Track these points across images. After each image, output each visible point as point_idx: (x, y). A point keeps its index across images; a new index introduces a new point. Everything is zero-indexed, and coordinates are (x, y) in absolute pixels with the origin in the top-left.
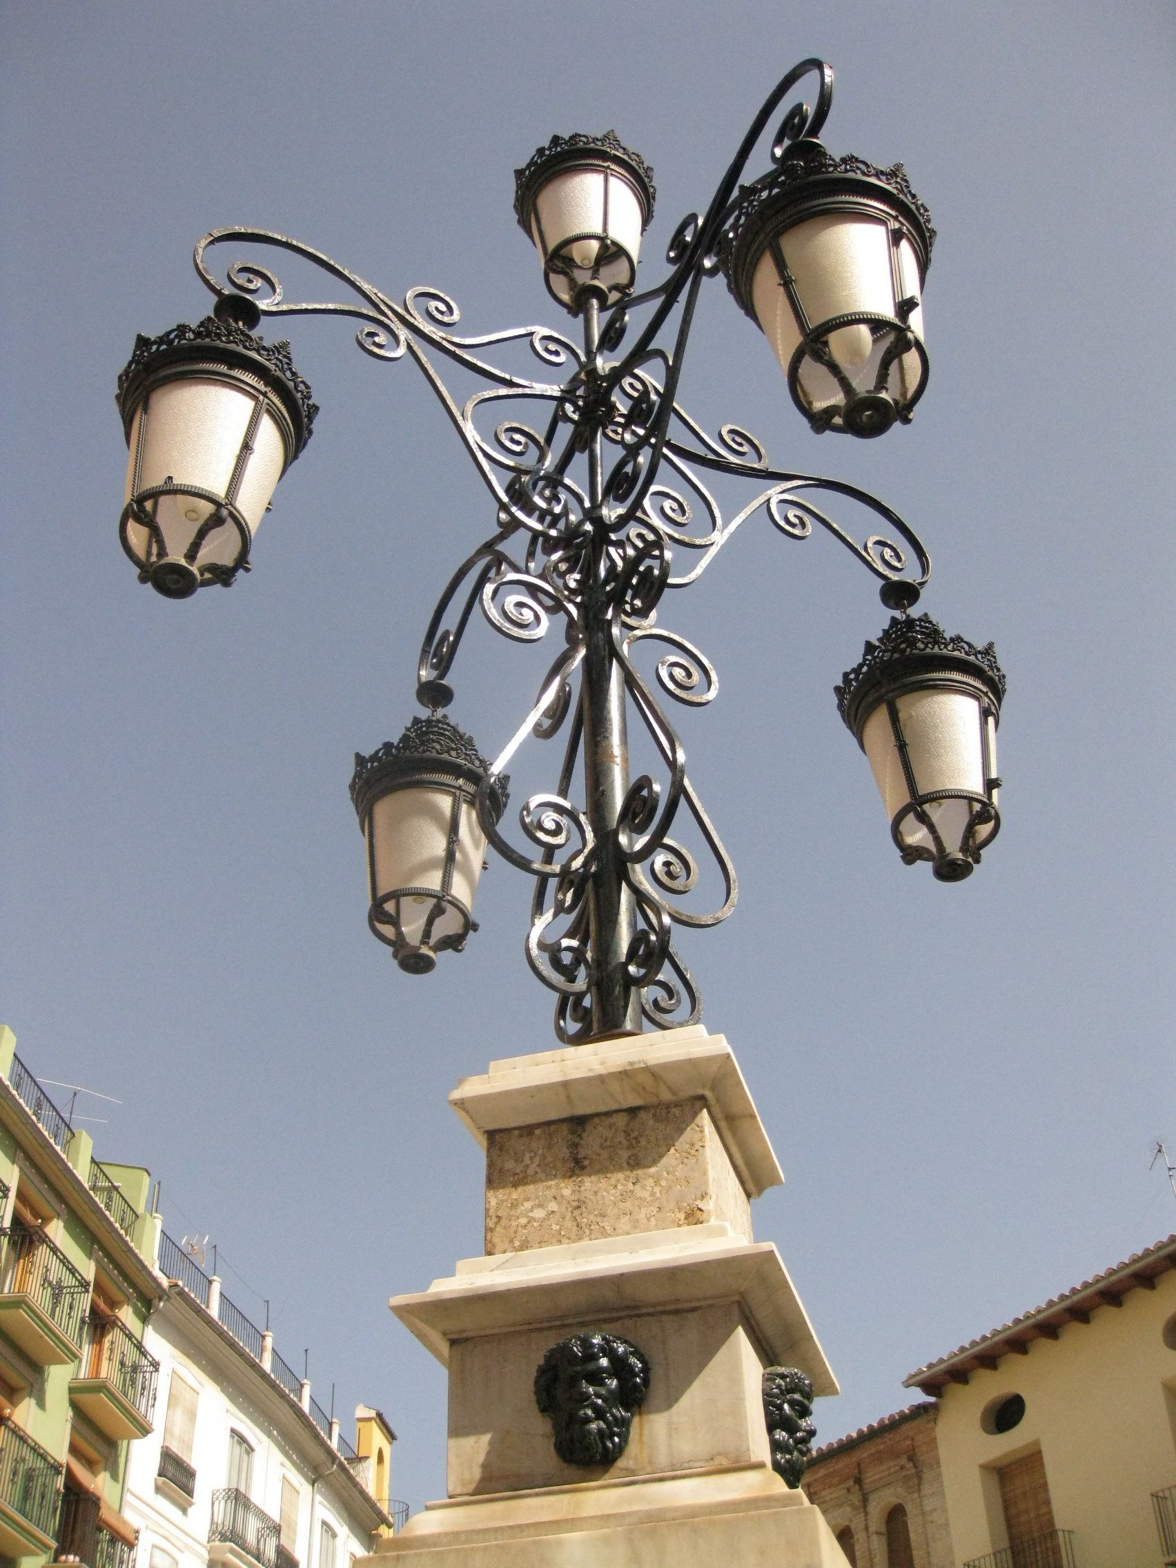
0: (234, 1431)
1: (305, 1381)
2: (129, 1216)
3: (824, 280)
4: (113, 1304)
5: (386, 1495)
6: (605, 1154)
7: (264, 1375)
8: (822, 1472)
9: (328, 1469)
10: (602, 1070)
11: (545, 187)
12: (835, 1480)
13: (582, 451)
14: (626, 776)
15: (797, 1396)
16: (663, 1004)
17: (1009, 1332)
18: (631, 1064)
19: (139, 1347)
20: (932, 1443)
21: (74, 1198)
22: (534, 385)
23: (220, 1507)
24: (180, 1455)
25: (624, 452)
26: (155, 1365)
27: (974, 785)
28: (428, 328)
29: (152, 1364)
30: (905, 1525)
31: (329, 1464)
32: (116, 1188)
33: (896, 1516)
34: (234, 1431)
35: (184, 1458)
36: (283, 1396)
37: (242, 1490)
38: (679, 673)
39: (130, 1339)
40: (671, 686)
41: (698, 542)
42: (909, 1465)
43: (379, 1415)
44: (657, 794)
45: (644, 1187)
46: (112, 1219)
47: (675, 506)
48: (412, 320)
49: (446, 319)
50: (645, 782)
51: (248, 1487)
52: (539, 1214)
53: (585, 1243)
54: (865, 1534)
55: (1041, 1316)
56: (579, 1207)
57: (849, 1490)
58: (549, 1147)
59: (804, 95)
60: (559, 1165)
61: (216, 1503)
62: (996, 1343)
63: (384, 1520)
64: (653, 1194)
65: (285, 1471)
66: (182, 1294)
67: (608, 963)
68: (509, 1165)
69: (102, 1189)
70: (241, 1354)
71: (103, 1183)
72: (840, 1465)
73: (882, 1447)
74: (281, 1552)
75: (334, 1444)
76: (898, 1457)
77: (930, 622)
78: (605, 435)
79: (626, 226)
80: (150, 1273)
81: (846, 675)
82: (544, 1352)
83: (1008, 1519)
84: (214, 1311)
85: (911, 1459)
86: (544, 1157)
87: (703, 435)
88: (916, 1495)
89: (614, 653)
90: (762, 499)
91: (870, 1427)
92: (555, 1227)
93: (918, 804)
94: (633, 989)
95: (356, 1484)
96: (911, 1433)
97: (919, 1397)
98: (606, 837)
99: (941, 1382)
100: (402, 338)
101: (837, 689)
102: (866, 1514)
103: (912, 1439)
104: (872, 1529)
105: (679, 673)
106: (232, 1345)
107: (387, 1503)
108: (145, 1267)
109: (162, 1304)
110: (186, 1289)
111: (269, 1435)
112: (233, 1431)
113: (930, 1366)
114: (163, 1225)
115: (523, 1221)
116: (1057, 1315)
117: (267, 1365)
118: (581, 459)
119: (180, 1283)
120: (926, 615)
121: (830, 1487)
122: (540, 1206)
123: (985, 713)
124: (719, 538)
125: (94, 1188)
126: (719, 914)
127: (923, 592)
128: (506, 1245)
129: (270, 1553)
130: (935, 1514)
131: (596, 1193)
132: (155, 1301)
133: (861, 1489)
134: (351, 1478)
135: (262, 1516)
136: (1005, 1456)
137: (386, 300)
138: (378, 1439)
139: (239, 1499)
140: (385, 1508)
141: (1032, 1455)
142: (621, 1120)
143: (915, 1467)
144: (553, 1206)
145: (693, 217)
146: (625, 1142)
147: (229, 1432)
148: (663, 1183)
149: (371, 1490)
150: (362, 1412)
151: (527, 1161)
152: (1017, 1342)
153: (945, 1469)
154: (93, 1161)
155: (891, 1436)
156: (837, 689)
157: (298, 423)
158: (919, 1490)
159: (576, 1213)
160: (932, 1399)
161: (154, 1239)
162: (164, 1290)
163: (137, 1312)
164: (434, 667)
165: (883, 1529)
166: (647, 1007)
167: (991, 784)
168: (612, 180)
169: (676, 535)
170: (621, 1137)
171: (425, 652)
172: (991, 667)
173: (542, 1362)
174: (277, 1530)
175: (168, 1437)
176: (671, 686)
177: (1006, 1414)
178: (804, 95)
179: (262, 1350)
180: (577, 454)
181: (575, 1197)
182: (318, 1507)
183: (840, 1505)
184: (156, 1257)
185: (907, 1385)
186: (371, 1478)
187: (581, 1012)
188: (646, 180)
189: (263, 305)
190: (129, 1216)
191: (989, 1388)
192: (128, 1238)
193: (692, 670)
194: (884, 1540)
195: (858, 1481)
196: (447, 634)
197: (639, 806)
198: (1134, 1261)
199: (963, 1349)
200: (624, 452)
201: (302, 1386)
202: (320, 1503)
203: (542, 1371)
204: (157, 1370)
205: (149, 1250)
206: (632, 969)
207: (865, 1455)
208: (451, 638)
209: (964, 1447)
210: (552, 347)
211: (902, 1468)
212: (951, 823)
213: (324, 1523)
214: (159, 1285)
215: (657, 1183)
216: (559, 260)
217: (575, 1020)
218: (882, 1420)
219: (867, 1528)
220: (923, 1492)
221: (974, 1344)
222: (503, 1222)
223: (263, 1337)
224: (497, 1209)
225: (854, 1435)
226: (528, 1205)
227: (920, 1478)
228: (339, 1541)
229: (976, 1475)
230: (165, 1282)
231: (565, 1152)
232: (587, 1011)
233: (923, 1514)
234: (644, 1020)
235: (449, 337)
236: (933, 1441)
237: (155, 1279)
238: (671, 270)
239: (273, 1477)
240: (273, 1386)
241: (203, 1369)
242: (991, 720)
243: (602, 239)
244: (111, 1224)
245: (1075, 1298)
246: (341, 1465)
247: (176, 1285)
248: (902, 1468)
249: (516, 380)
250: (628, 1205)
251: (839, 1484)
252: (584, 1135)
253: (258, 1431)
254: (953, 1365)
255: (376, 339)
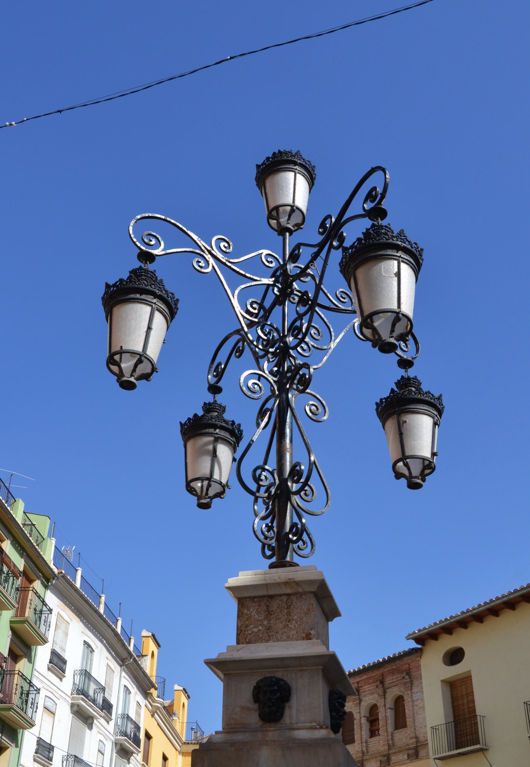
0: (85, 642)
1: (119, 618)
2: (40, 539)
3: (374, 288)
4: (31, 581)
5: (154, 674)
6: (279, 610)
7: (100, 616)
8: (364, 677)
9: (128, 660)
10: (279, 581)
11: (270, 175)
12: (370, 681)
13: (280, 305)
14: (291, 461)
15: (340, 700)
16: (301, 547)
17: (458, 618)
18: (289, 579)
19: (43, 602)
20: (419, 667)
21: (15, 531)
22: (262, 279)
23: (77, 678)
24: (60, 653)
25: (297, 316)
26: (50, 610)
27: (427, 454)
28: (220, 256)
29: (49, 610)
30: (403, 706)
31: (129, 658)
32: (34, 525)
33: (399, 701)
34: (85, 642)
35: (62, 655)
36: (109, 626)
37: (88, 670)
38: (313, 408)
39: (39, 598)
40: (310, 414)
41: (325, 347)
42: (407, 677)
43: (153, 635)
44: (303, 470)
45: (292, 624)
46: (33, 541)
47: (316, 332)
48: (216, 254)
49: (228, 251)
50: (298, 464)
51: (91, 669)
52: (256, 630)
53: (270, 643)
54: (384, 708)
55: (475, 611)
56: (268, 629)
57: (377, 686)
58: (260, 606)
59: (376, 181)
60: (263, 613)
61: (76, 676)
62: (452, 623)
63: (153, 686)
64: (295, 626)
65: (108, 661)
66: (63, 577)
67: (282, 532)
68: (245, 611)
69: (28, 525)
70: (91, 606)
71: (28, 522)
72: (373, 674)
73: (394, 667)
74: (105, 700)
75: (131, 648)
76: (402, 672)
77: (417, 380)
78: (289, 300)
79: (302, 201)
80: (49, 567)
81: (381, 400)
82: (256, 681)
83: (454, 707)
84: (78, 585)
85: (408, 674)
86: (257, 609)
87: (329, 295)
88: (409, 692)
89: (289, 404)
90: (351, 324)
91: (389, 657)
92: (261, 635)
93: (404, 458)
94: (291, 544)
95: (141, 669)
96: (409, 662)
97: (413, 645)
98: (283, 482)
99: (425, 638)
100: (210, 263)
101: (377, 403)
102: (385, 699)
103: (409, 665)
104: (388, 706)
105: (313, 408)
106: (86, 601)
107: (155, 677)
108: (47, 563)
109: (54, 582)
110: (104, 616)
111: (102, 642)
112: (84, 641)
113: (419, 631)
114: (82, 573)
115: (250, 632)
116: (482, 611)
117: (102, 610)
118: (278, 309)
119: (63, 572)
120: (416, 376)
121: (368, 684)
122: (255, 627)
123: (435, 424)
124: (333, 345)
125: (24, 525)
126: (323, 510)
127: (415, 361)
128: (243, 641)
129: (100, 700)
130: (419, 701)
131: (275, 624)
132: (51, 580)
133: (383, 686)
134: (139, 665)
135: (97, 682)
136: (452, 677)
137: (204, 244)
138: (152, 647)
139: (86, 674)
140: (154, 680)
141: (467, 677)
142: (285, 598)
143: (410, 678)
144: (260, 628)
145: (330, 217)
146: (286, 607)
147: (83, 642)
148: (299, 623)
149: (148, 671)
150: (145, 633)
151: (252, 610)
152: (463, 623)
153: (424, 680)
154: (24, 512)
155: (398, 662)
156: (377, 403)
157: (171, 311)
158: (411, 689)
159: (268, 631)
160: (420, 646)
161: (51, 550)
162: (55, 575)
163: (42, 583)
164: (215, 376)
165: (393, 707)
166: (295, 549)
167: (434, 454)
168: (298, 176)
169: (316, 346)
170: (284, 605)
171: (210, 367)
172: (439, 404)
173: (255, 684)
174: (103, 689)
175: (54, 645)
176: (310, 414)
177: (455, 657)
178: (376, 181)
179: (100, 603)
180: (277, 306)
181: (268, 625)
182: (123, 679)
183: (372, 694)
184: (52, 558)
185: (408, 638)
186: (149, 666)
187: (271, 548)
188: (312, 172)
189: (156, 252)
190: (40, 539)
191: (448, 643)
192: (40, 550)
193: (319, 407)
194: (393, 711)
195: (382, 682)
196: (220, 364)
197: (295, 472)
198: (522, 589)
199: (435, 624)
200: (297, 316)
201: (117, 620)
202: (124, 677)
203: (255, 688)
204: (51, 613)
205: (48, 554)
206: (290, 536)
207: (386, 670)
208: (223, 366)
209: (433, 671)
210: (270, 259)
211: (403, 678)
212: (416, 468)
213: (125, 686)
214: (53, 572)
215: (296, 622)
216: (274, 212)
217: (269, 550)
218: (395, 654)
219: (385, 706)
220: (413, 691)
221: (441, 622)
222: (243, 632)
223: (100, 597)
224: (241, 627)
225: (381, 660)
226: (252, 626)
227: (412, 683)
228: (132, 695)
229: (439, 685)
230: (56, 571)
231: (265, 608)
232: (273, 547)
233: (413, 701)
234: (294, 553)
235: (229, 260)
236: (419, 666)
237: (51, 570)
238: (321, 238)
239: (103, 665)
240: (105, 621)
241: (72, 611)
242: (437, 426)
243: (292, 207)
244: (32, 543)
245: (492, 604)
246: (135, 660)
247: (61, 573)
248: (403, 678)
249: (255, 278)
250: (286, 630)
251: (373, 683)
252: (272, 602)
253: (96, 640)
254: (430, 631)
255: (200, 264)
